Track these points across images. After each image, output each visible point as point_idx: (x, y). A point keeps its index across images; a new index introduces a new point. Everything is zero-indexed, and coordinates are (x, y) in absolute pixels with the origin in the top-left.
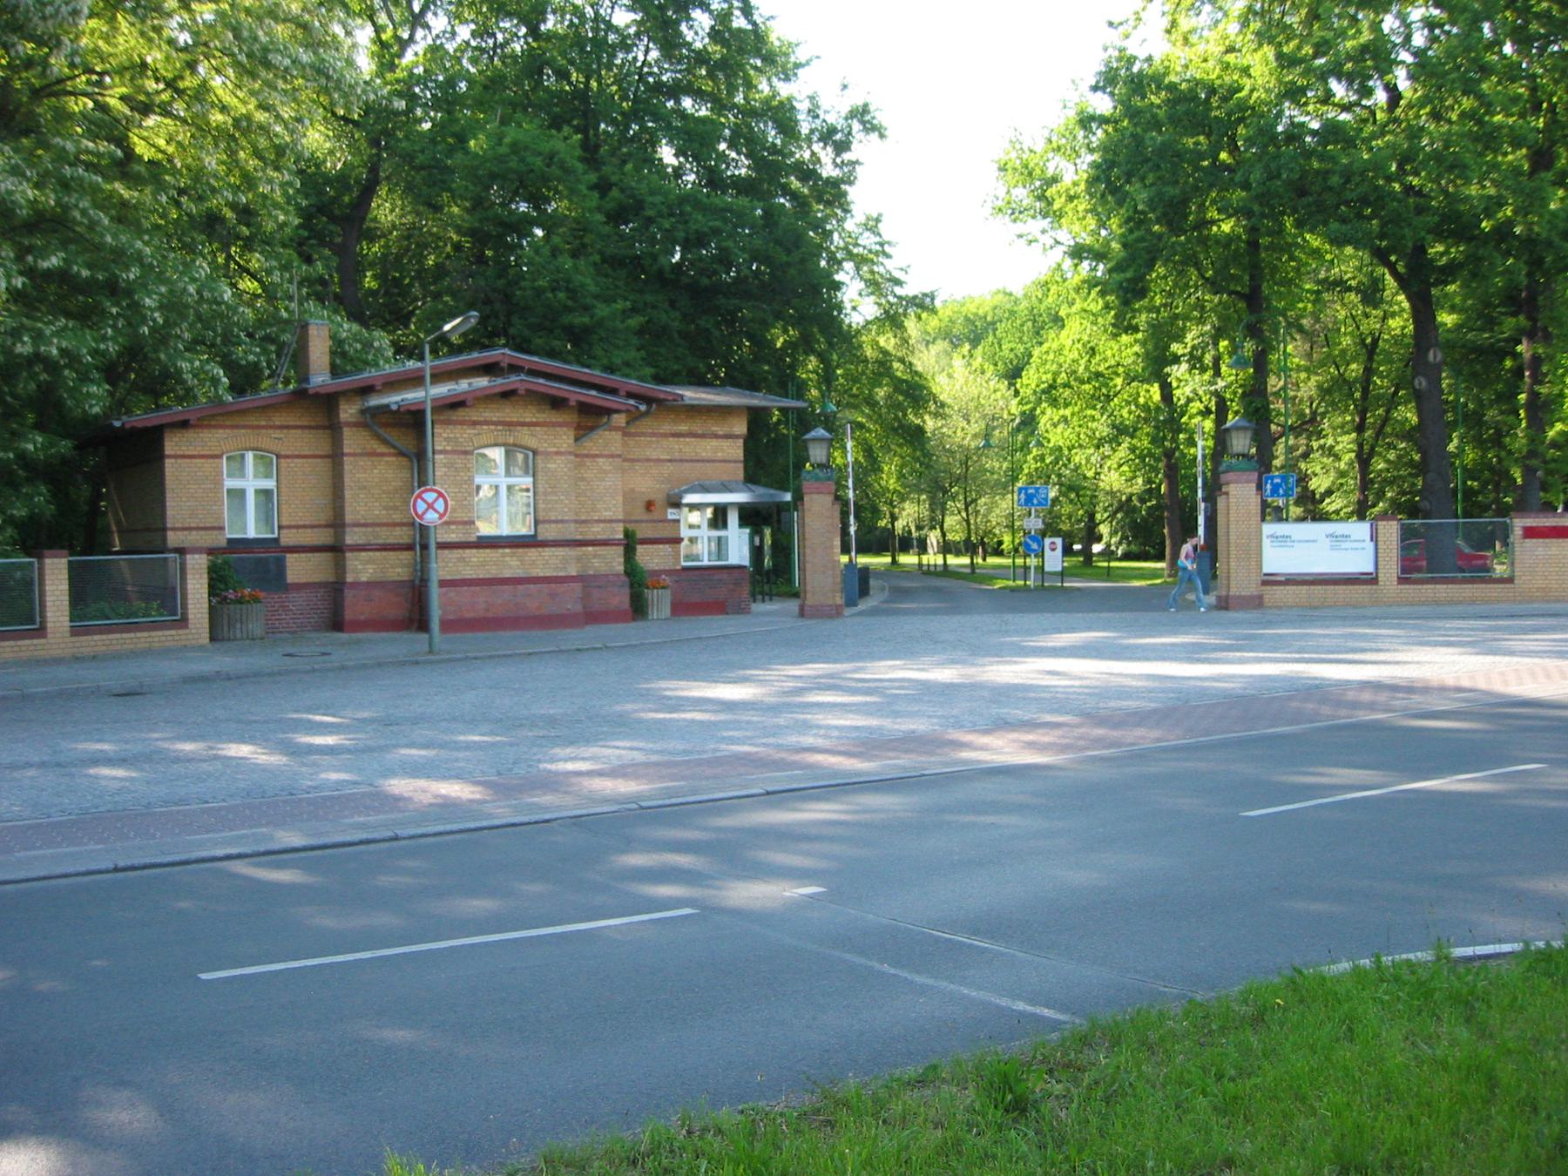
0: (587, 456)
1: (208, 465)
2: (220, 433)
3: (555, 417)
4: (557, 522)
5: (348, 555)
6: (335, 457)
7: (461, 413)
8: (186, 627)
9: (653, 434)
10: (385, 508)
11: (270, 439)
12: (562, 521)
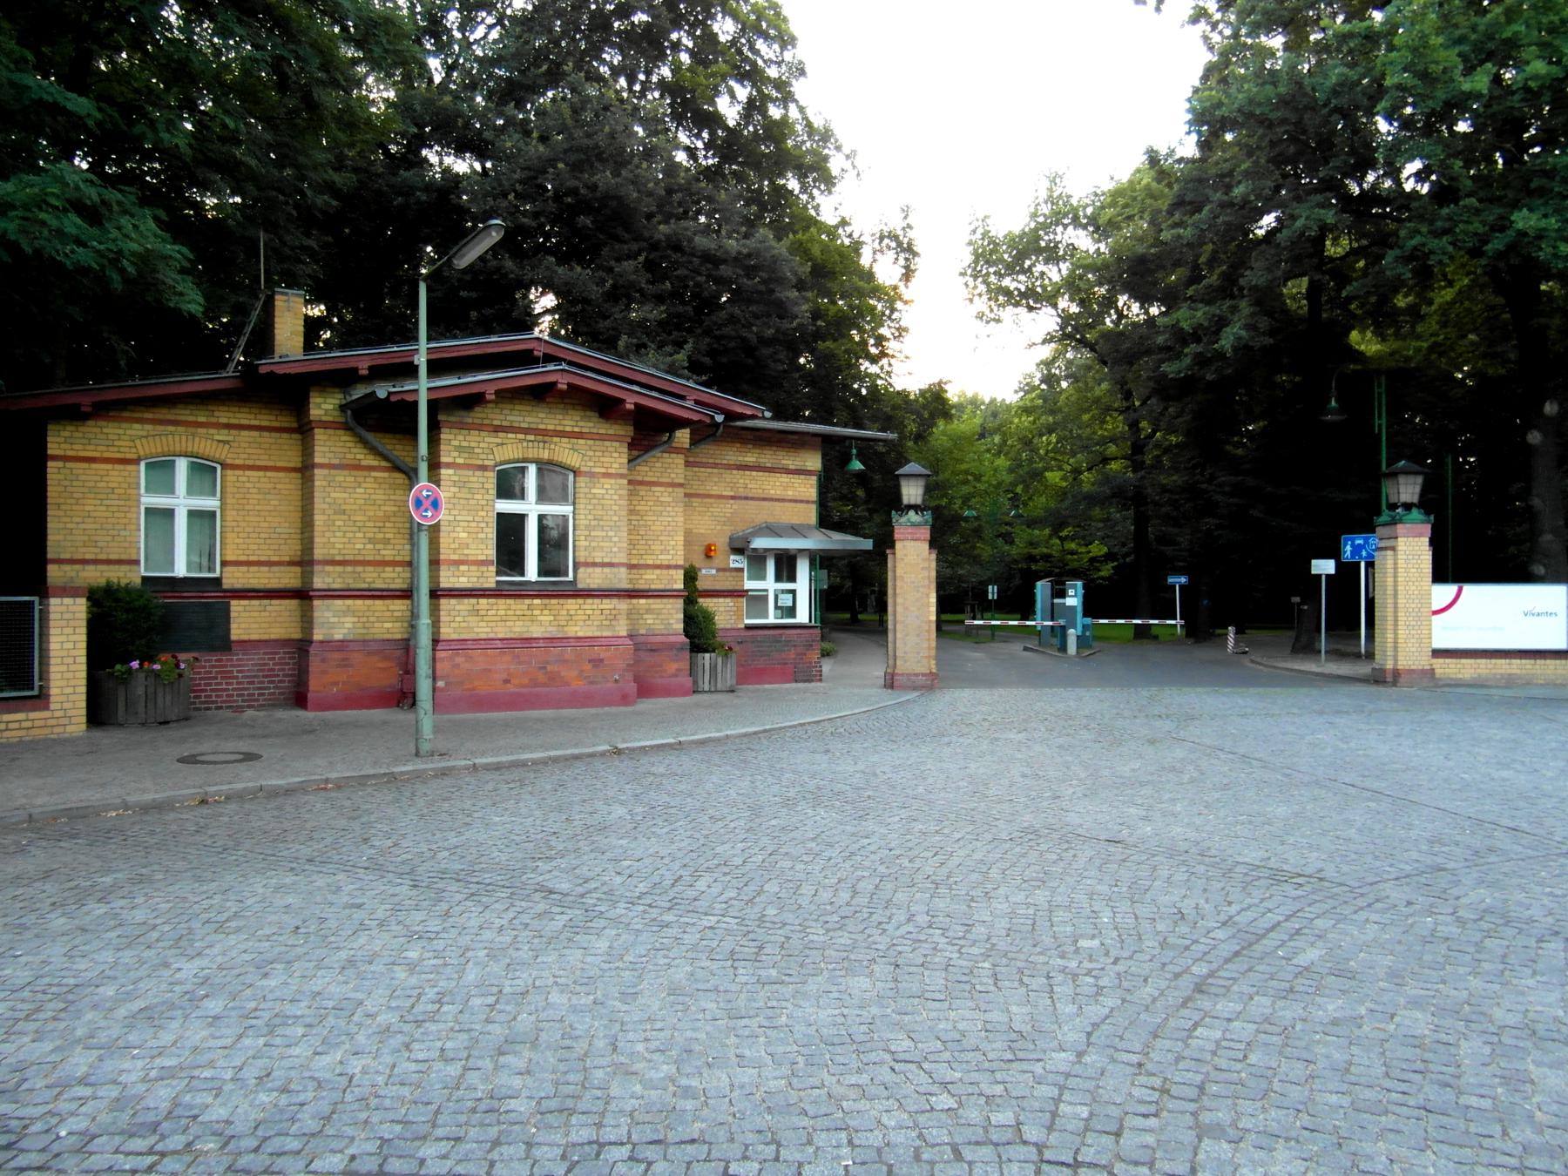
0: (642, 483)
1: (116, 474)
2: (137, 429)
3: (604, 428)
4: (603, 565)
5: (316, 603)
6: (306, 469)
7: (478, 414)
8: (46, 708)
9: (715, 466)
10: (371, 541)
11: (209, 443)
12: (611, 565)
